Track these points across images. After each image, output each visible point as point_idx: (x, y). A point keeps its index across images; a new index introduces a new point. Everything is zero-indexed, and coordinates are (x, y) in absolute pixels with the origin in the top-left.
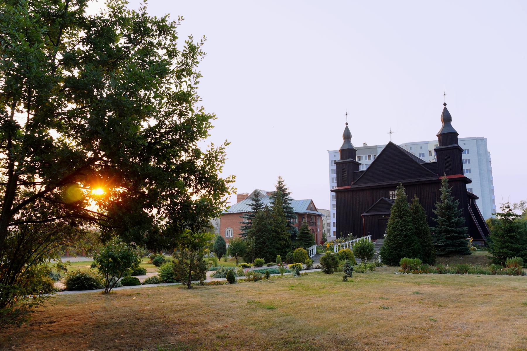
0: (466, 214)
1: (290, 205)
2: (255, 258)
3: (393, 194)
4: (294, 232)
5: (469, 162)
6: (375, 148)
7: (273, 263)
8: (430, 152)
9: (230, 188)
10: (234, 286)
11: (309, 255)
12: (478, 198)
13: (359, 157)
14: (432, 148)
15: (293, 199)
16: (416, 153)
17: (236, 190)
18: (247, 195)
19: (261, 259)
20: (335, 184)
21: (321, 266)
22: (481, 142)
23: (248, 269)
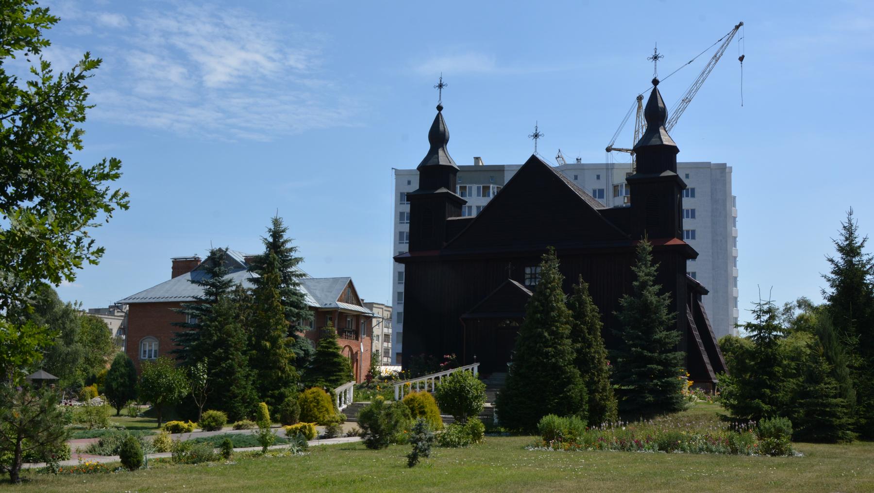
0: (681, 324)
1: (298, 288)
2: (205, 410)
3: (531, 274)
4: (304, 350)
5: (693, 216)
6: (499, 170)
7: (246, 422)
8: (616, 188)
9: (110, 193)
10: (135, 477)
11: (334, 404)
12: (706, 292)
13: (463, 189)
14: (620, 179)
15: (304, 275)
16: (585, 190)
17: (126, 199)
18: (196, 260)
19: (219, 413)
20: (405, 248)
21: (361, 431)
22: (731, 168)
23: (179, 435)
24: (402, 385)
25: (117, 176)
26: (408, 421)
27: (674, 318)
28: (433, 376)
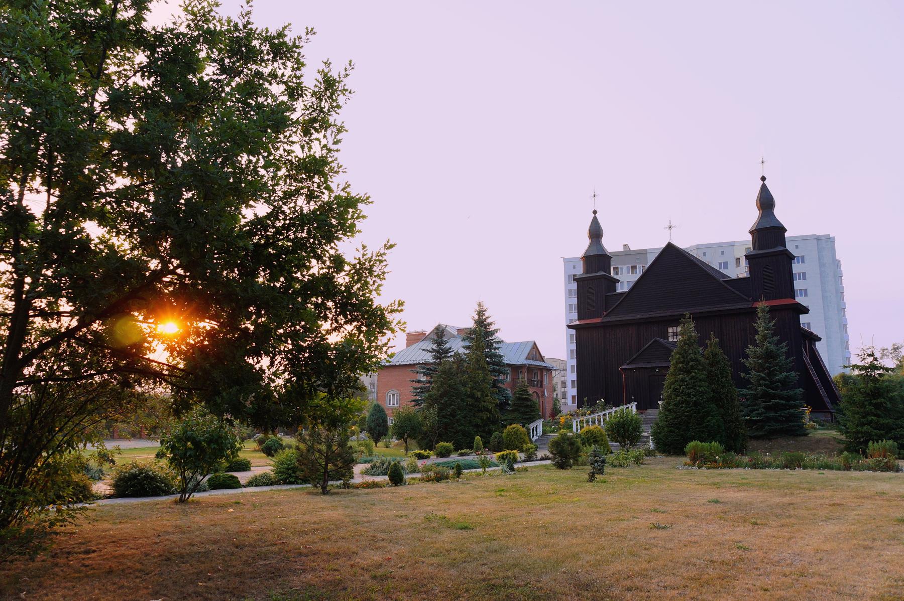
1: (497, 351)
2: (437, 442)
3: (673, 333)
4: (505, 397)
6: (643, 253)
8: (738, 260)
9: (395, 322)
10: (401, 490)
11: (530, 436)
12: (819, 339)
13: (616, 269)
14: (741, 253)
15: (502, 341)
16: (713, 261)
17: (405, 326)
18: (423, 334)
21: (551, 456)
22: (825, 243)
23: (424, 460)
24: (579, 420)
25: (402, 310)
26: (585, 448)
27: (791, 362)
28: (602, 414)
